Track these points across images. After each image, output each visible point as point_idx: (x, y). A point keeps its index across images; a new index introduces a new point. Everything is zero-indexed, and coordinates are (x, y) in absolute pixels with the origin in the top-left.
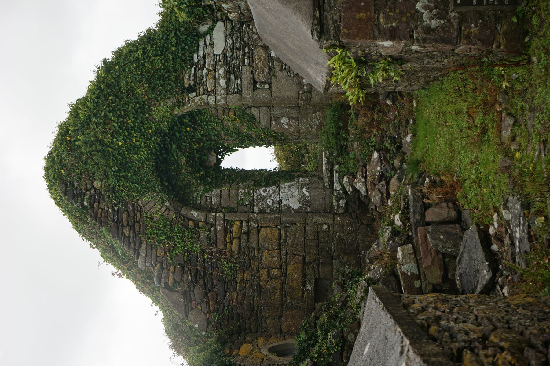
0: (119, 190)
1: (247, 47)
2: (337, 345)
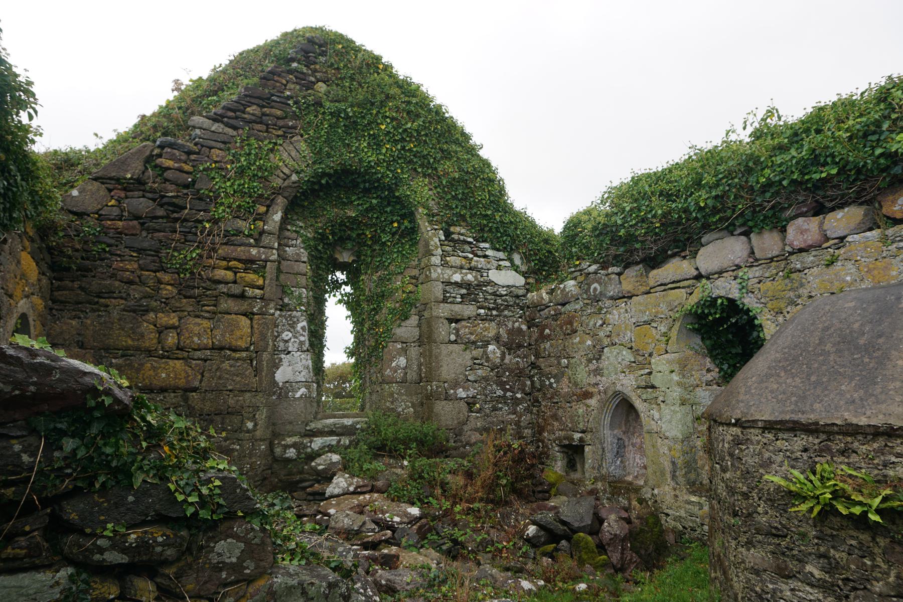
0: (318, 112)
2: (203, 502)
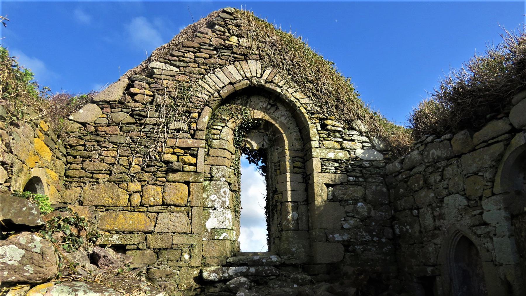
1: (363, 180)
